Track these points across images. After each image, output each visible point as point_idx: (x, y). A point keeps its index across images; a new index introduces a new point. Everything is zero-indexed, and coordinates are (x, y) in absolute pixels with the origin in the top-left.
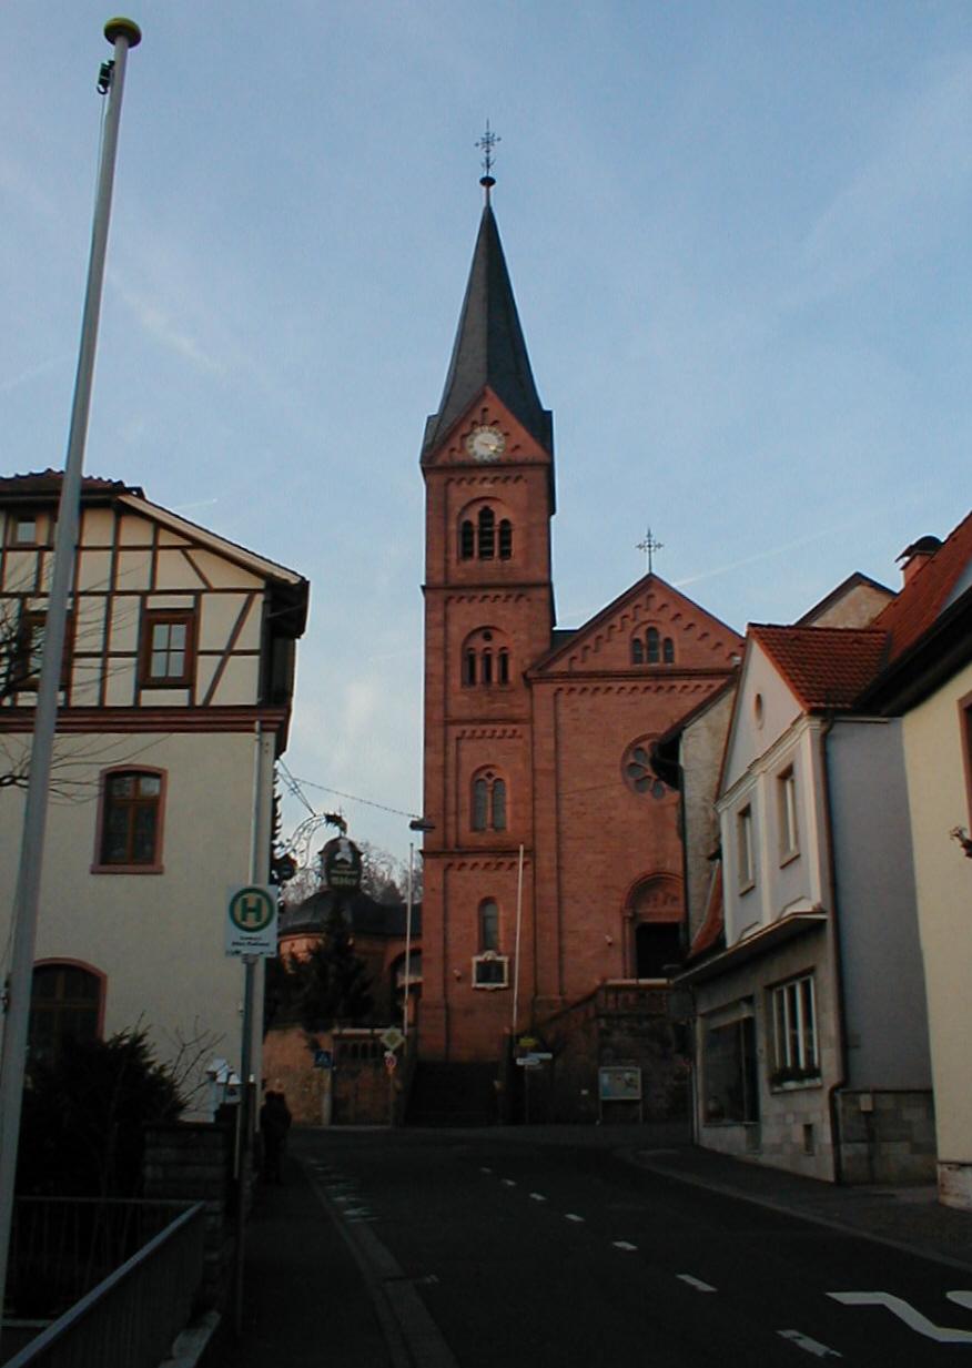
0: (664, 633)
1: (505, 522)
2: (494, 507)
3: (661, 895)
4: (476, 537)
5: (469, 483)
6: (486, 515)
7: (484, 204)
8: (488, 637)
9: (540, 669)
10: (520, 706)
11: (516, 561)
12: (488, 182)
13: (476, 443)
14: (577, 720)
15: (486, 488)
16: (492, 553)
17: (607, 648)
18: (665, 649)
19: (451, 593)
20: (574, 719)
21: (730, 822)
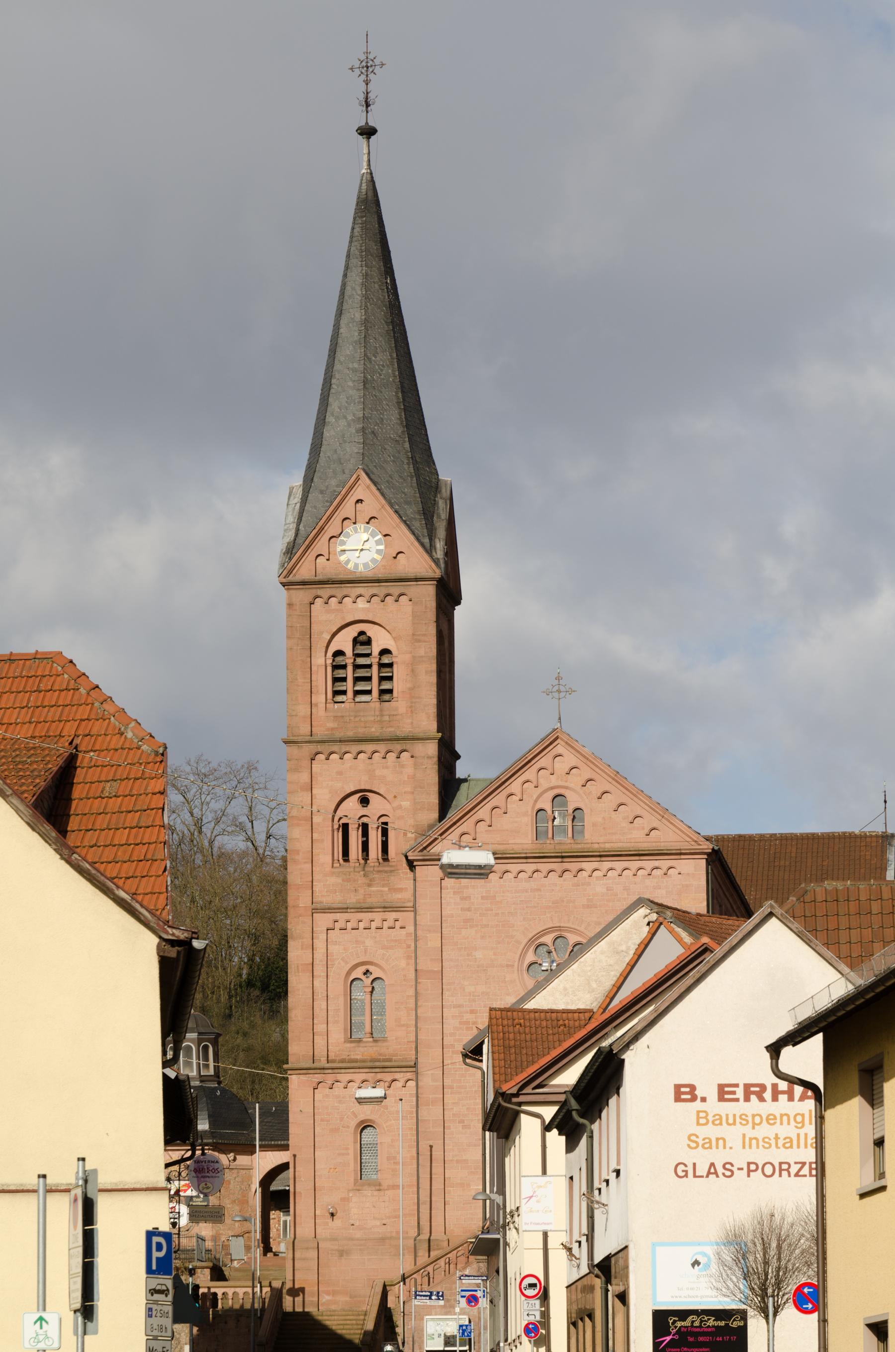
1: (385, 652)
2: (371, 631)
6: (362, 641)
8: (365, 801)
14: (469, 910)
15: (361, 608)
20: (462, 909)
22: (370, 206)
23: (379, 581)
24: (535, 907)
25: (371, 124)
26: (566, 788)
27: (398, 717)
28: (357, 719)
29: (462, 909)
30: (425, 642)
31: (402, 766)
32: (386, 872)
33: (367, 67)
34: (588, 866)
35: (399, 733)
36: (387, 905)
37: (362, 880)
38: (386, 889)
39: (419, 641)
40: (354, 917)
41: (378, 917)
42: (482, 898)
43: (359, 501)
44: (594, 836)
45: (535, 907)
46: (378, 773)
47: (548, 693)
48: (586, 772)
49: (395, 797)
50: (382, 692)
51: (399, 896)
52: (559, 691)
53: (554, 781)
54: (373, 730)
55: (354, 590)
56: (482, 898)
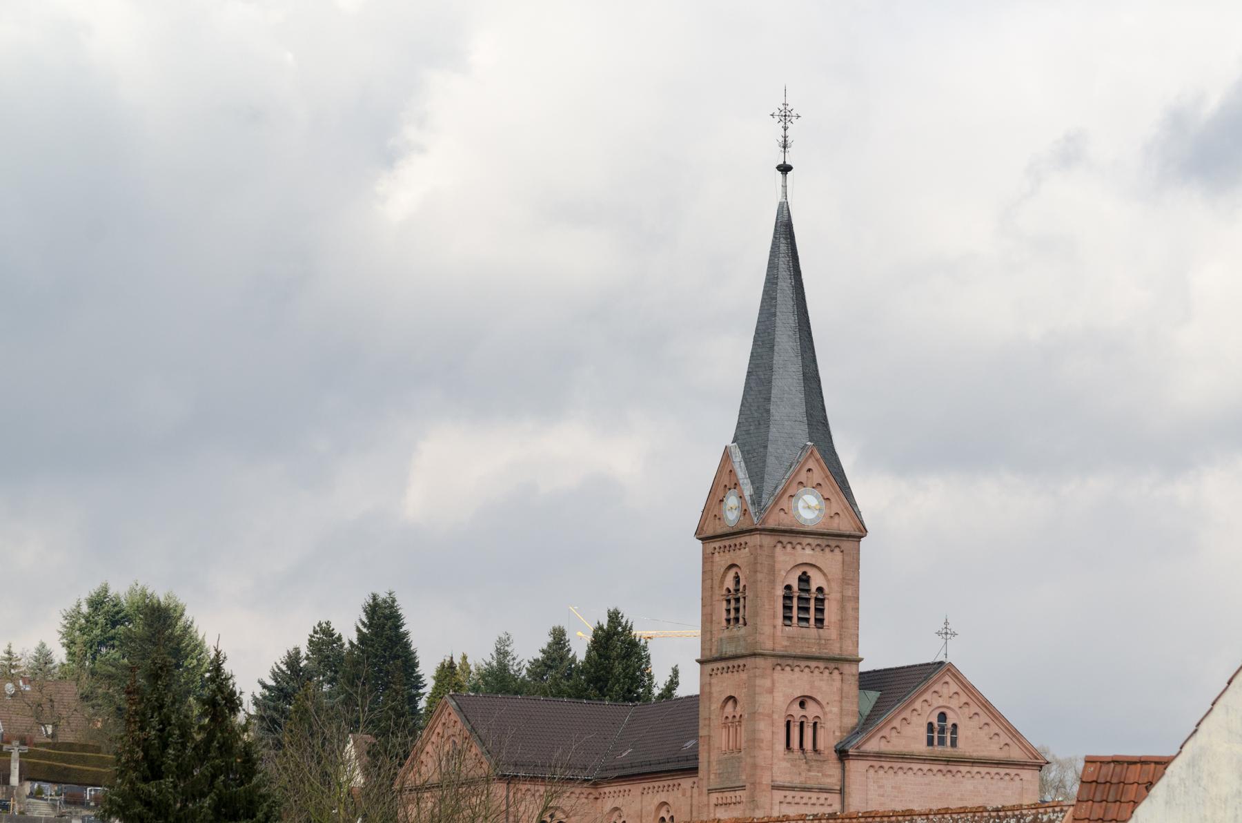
1: (820, 590)
2: (811, 572)
3: (838, 734)
4: (795, 600)
6: (804, 579)
7: (779, 198)
8: (802, 704)
12: (785, 169)
13: (801, 504)
17: (908, 731)
22: (785, 230)
23: (822, 534)
34: (964, 769)
35: (831, 655)
37: (804, 766)
40: (798, 794)
41: (814, 795)
43: (809, 470)
51: (829, 780)
53: (941, 702)
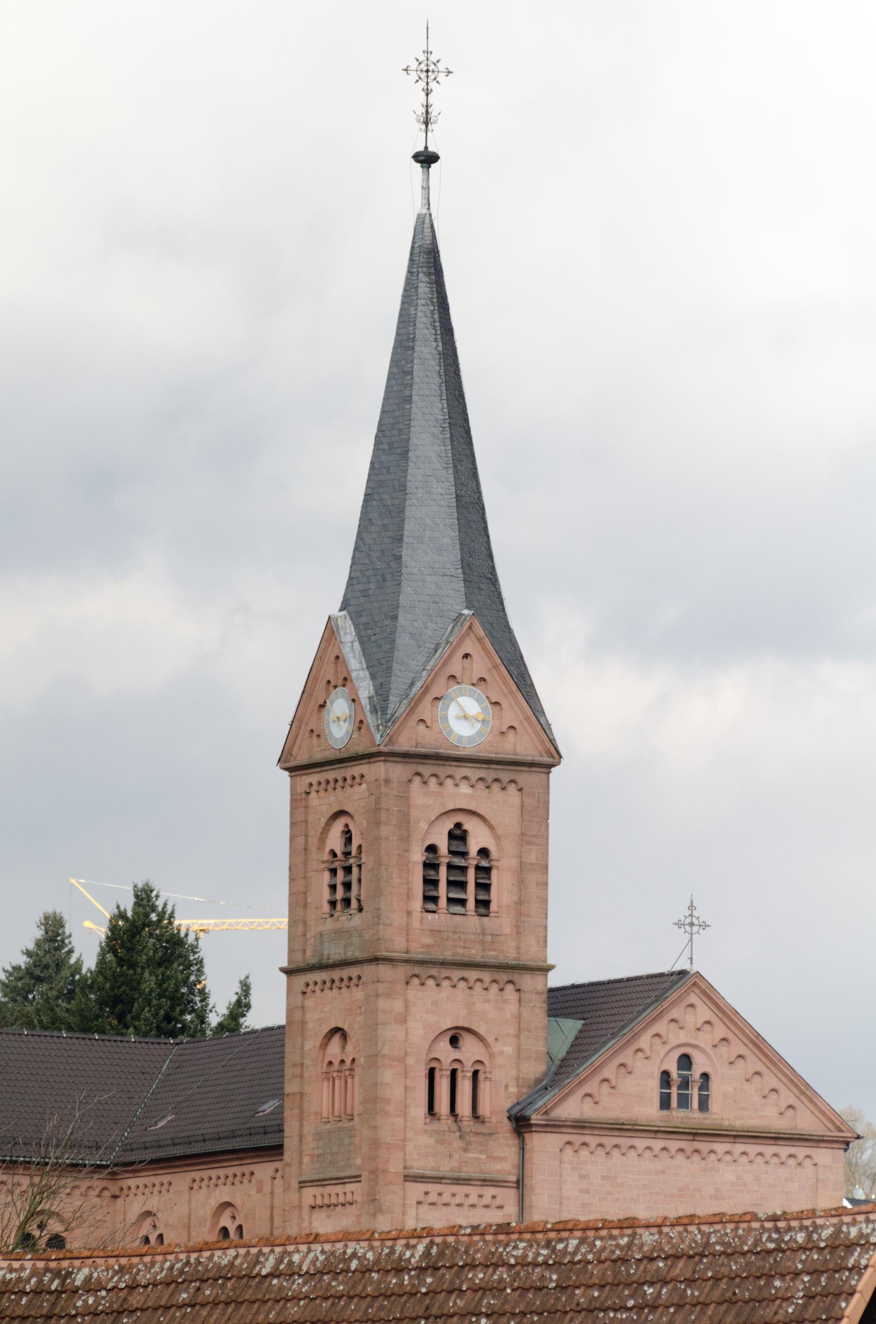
0: (700, 1065)
1: (484, 852)
2: (470, 824)
5: (666, 1074)
6: (458, 835)
9: (546, 1113)
10: (500, 1159)
11: (501, 919)
13: (453, 711)
14: (587, 1191)
15: (461, 794)
16: (462, 902)
18: (700, 1089)
19: (417, 970)
20: (581, 1191)
21: (858, 1303)
22: (426, 261)
23: (488, 762)
24: (658, 1194)
25: (431, 149)
26: (695, 1046)
27: (502, 938)
28: (456, 936)
29: (581, 1191)
30: (536, 844)
31: (505, 1001)
32: (484, 1134)
33: (427, 71)
34: (721, 1147)
35: (502, 959)
36: (486, 1176)
37: (457, 1144)
38: (484, 1157)
39: (530, 843)
41: (474, 1191)
42: (603, 1177)
43: (466, 656)
44: (723, 1111)
45: (658, 1194)
46: (479, 1007)
47: (679, 924)
48: (720, 1031)
49: (496, 1039)
50: (478, 902)
52: (692, 924)
53: (683, 1037)
54: (473, 951)
55: (459, 769)
56: (603, 1177)
